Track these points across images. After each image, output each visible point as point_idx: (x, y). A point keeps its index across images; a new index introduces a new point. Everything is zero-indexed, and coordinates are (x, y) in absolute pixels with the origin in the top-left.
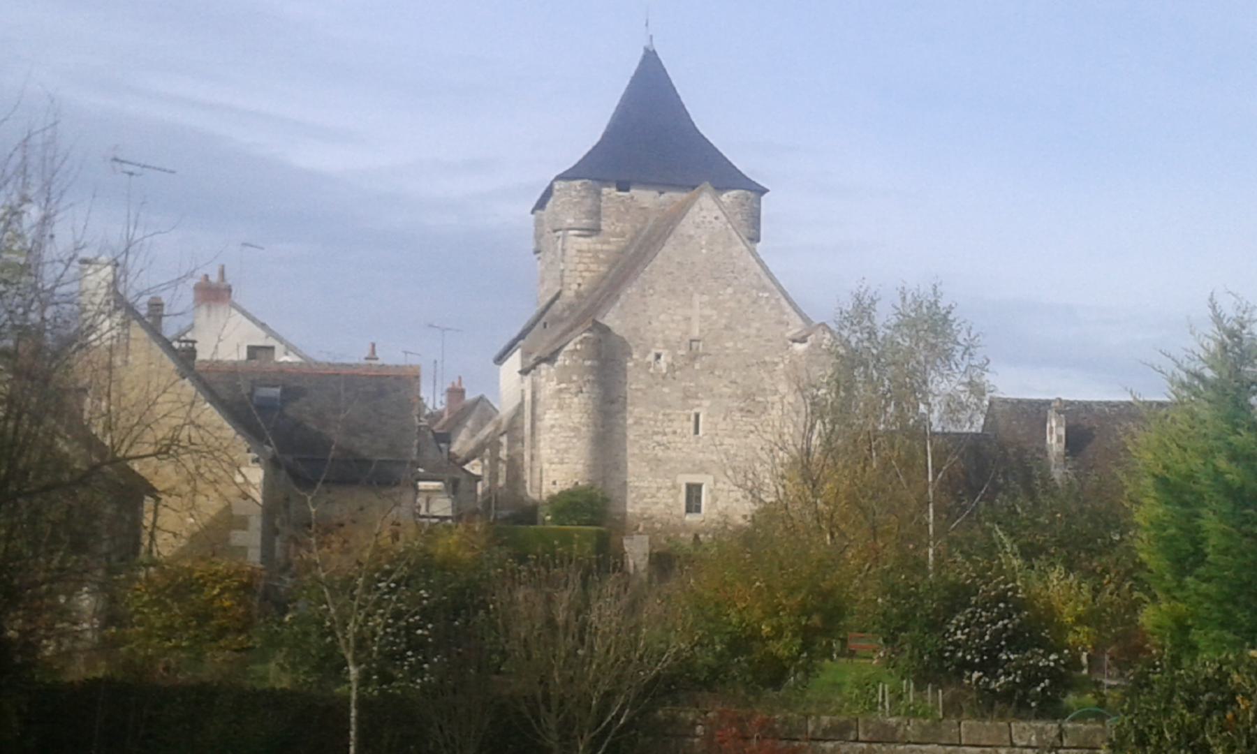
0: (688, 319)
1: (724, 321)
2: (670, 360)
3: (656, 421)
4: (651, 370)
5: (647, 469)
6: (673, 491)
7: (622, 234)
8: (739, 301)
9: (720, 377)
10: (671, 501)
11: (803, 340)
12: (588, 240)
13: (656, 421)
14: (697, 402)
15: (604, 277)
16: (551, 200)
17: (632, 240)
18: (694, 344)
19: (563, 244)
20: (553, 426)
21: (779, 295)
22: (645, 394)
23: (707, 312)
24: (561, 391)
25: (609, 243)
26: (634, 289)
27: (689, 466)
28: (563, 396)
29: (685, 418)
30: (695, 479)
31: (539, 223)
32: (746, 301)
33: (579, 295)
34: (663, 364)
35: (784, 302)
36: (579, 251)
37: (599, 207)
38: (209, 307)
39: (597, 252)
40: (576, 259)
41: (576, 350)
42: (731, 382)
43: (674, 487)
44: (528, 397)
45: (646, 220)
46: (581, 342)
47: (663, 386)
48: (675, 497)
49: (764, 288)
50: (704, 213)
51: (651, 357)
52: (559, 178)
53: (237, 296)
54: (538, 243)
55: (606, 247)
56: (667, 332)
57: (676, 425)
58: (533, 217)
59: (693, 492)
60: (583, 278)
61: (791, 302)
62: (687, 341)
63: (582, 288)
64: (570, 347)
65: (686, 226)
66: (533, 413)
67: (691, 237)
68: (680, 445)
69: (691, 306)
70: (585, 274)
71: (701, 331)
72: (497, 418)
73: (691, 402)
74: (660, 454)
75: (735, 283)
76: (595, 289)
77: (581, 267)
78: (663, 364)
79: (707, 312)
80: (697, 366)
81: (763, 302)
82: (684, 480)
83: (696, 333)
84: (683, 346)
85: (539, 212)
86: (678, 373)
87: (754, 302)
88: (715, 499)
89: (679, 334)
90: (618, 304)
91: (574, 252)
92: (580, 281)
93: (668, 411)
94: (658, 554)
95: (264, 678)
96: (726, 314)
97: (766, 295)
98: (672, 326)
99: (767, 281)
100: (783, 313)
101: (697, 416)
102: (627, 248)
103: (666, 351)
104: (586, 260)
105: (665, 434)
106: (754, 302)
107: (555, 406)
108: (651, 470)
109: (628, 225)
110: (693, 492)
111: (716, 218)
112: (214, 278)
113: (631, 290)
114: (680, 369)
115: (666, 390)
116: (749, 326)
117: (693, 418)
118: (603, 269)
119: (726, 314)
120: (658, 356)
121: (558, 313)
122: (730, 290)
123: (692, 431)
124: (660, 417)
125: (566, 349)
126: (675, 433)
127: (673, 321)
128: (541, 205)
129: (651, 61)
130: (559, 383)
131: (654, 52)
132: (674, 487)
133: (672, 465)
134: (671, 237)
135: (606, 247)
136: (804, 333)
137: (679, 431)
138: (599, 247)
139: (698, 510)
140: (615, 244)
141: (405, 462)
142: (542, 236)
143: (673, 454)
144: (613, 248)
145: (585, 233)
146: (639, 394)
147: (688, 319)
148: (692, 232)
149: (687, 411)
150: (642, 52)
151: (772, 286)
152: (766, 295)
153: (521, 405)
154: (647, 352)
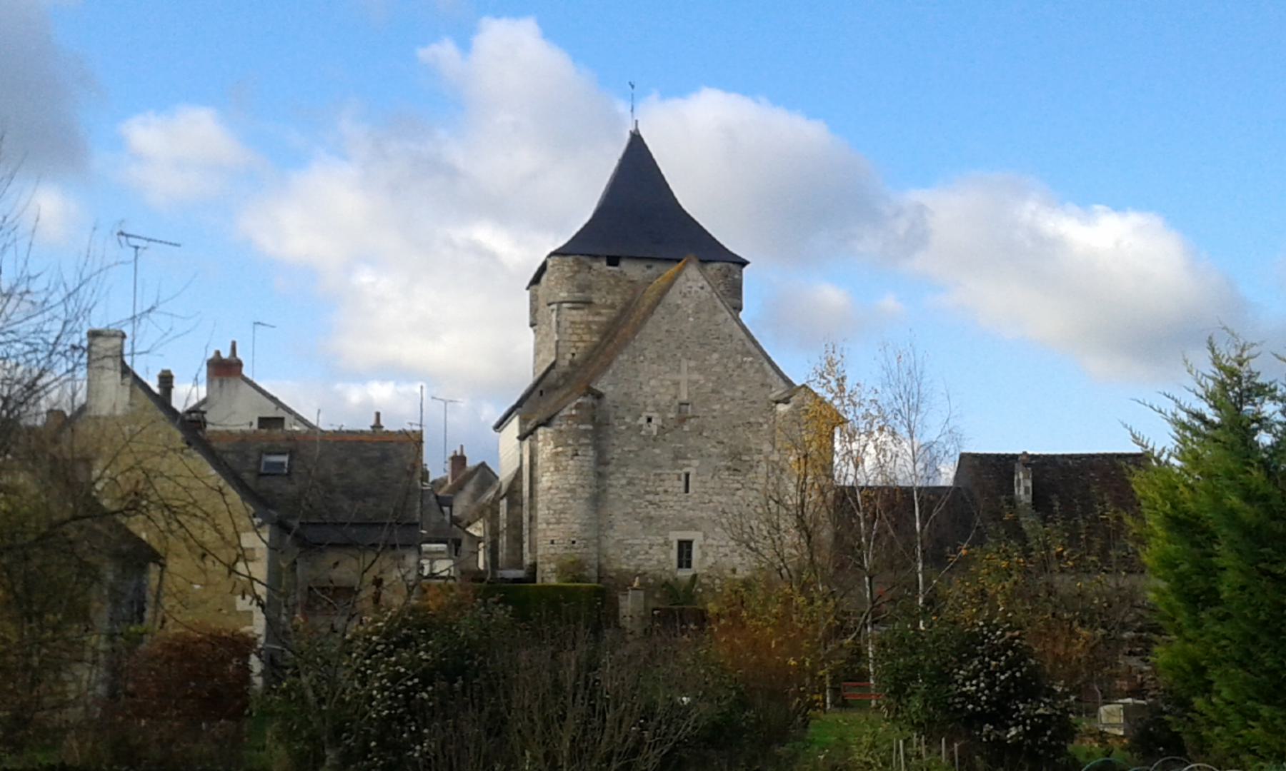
0: (676, 384)
2: (660, 422)
7: (612, 306)
12: (581, 312)
14: (686, 462)
18: (684, 407)
22: (637, 455)
23: (695, 376)
25: (598, 314)
26: (625, 357)
30: (686, 536)
31: (534, 299)
33: (572, 363)
34: (654, 427)
36: (573, 323)
39: (588, 324)
40: (570, 331)
46: (576, 407)
49: (748, 353)
51: (643, 421)
55: (597, 319)
57: (667, 484)
62: (676, 403)
63: (576, 357)
65: (673, 297)
71: (689, 394)
73: (680, 462)
74: (653, 513)
77: (575, 338)
79: (695, 376)
80: (686, 428)
82: (675, 536)
91: (568, 324)
92: (573, 350)
100: (766, 375)
101: (687, 475)
104: (579, 331)
109: (618, 297)
112: (226, 354)
114: (670, 431)
115: (657, 451)
117: (683, 477)
120: (649, 420)
122: (715, 356)
123: (682, 490)
126: (666, 491)
127: (662, 386)
133: (664, 522)
135: (597, 319)
138: (591, 318)
142: (536, 310)
143: (665, 513)
144: (603, 319)
146: (632, 455)
149: (678, 471)
153: (520, 470)
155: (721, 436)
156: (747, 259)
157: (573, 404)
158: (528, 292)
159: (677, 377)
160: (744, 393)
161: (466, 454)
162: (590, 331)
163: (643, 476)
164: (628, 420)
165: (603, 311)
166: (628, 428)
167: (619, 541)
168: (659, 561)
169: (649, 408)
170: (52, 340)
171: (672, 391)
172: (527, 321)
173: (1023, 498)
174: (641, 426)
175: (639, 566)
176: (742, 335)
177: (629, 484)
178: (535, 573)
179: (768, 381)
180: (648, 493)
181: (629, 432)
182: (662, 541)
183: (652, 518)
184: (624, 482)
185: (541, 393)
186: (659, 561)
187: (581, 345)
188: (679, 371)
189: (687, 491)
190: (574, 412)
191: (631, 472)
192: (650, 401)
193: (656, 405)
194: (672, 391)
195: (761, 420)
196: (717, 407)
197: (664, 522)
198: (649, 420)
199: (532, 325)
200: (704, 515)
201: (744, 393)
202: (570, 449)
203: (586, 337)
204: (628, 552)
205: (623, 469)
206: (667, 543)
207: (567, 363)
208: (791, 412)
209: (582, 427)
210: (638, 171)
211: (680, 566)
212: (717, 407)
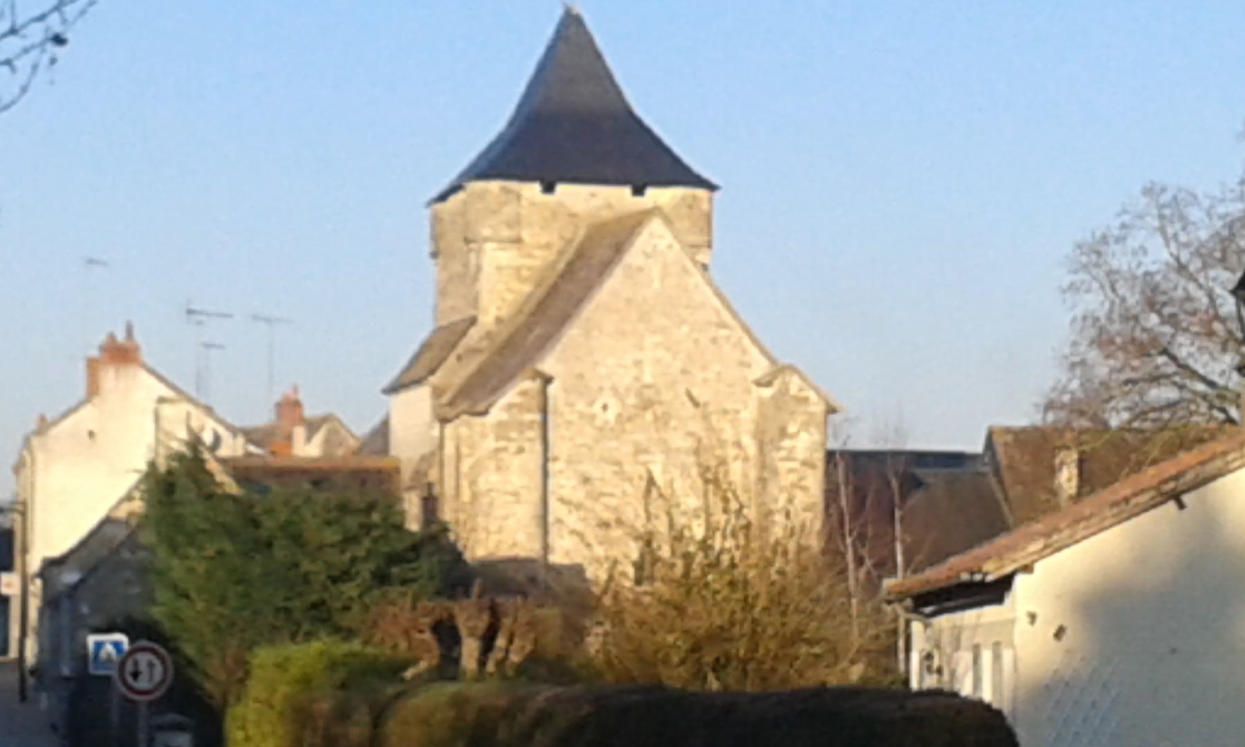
0: (638, 363)
7: (548, 246)
8: (696, 341)
11: (768, 384)
15: (530, 296)
17: (561, 253)
23: (661, 353)
24: (498, 450)
25: (530, 256)
31: (436, 220)
33: (499, 320)
34: (611, 415)
35: (746, 341)
38: (117, 370)
39: (518, 269)
45: (577, 227)
49: (723, 325)
51: (597, 408)
53: (146, 355)
55: (528, 262)
58: (427, 212)
61: (755, 342)
69: (641, 349)
72: (406, 476)
83: (648, 379)
95: (785, 680)
99: (727, 317)
100: (744, 352)
102: (555, 262)
112: (121, 337)
114: (630, 419)
118: (527, 288)
120: (605, 407)
122: (685, 329)
129: (571, 25)
135: (528, 262)
140: (540, 259)
144: (537, 263)
154: (591, 403)
156: (559, 13)
159: (639, 355)
161: (301, 396)
162: (522, 280)
165: (538, 253)
171: (634, 372)
172: (427, 248)
173: (1066, 485)
176: (716, 303)
179: (746, 359)
188: (641, 349)
192: (607, 384)
193: (615, 390)
194: (634, 372)
195: (738, 406)
198: (605, 407)
203: (516, 285)
208: (773, 398)
210: (572, 45)
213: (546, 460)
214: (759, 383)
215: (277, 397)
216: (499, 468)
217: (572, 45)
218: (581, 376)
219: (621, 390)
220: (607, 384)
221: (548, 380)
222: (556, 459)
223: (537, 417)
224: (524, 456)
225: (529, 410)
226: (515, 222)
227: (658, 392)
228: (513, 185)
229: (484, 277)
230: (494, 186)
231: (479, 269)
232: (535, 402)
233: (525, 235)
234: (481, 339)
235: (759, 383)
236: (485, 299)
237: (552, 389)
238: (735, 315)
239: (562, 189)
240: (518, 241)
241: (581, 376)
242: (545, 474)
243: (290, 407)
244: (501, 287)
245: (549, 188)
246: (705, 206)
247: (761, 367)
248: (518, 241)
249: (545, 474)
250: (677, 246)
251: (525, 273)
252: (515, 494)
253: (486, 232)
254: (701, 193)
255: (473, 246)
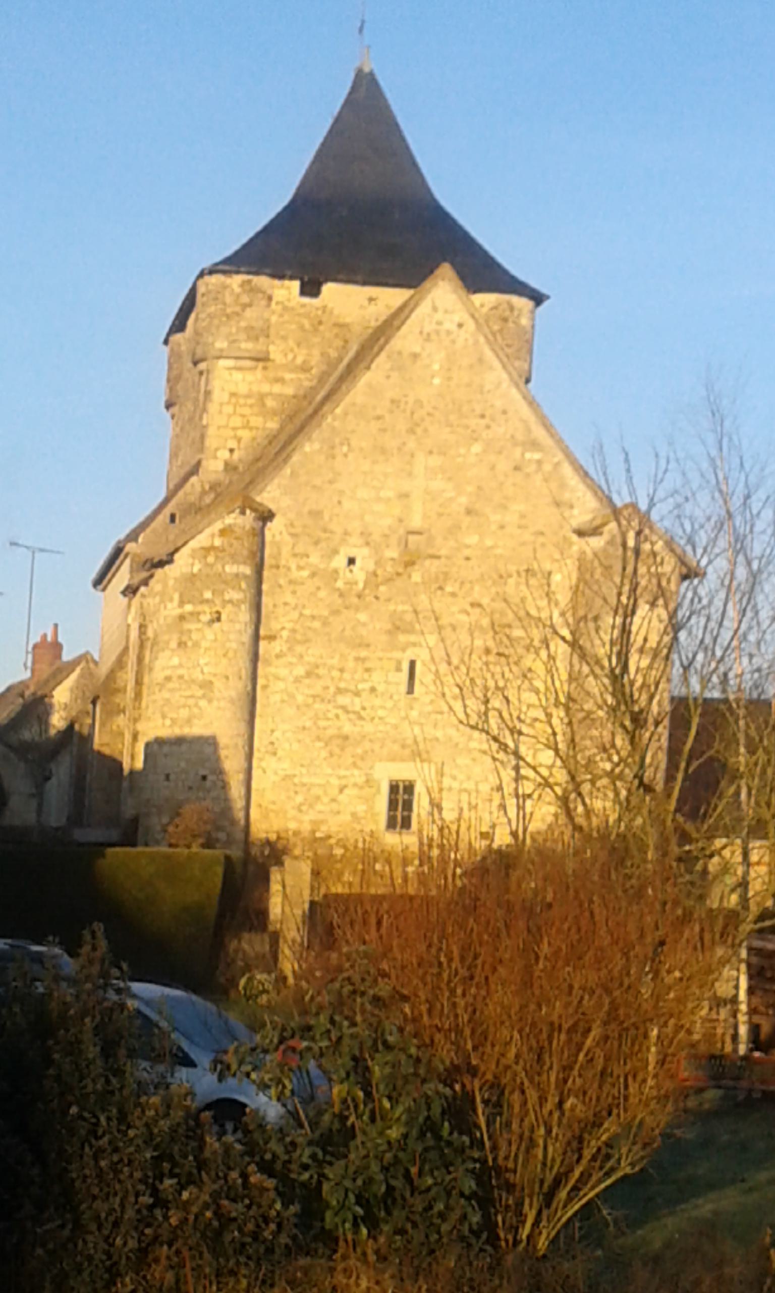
1: (463, 500)
2: (371, 567)
3: (342, 670)
4: (340, 584)
5: (324, 754)
6: (367, 791)
7: (305, 368)
9: (453, 595)
10: (361, 808)
12: (250, 377)
13: (342, 670)
14: (413, 638)
16: (193, 316)
18: (411, 538)
19: (207, 384)
20: (168, 679)
21: (560, 456)
22: (325, 623)
23: (438, 484)
24: (182, 618)
25: (280, 380)
26: (317, 446)
27: (396, 747)
28: (187, 626)
29: (393, 665)
30: (403, 772)
31: (174, 358)
32: (503, 465)
33: (229, 467)
34: (359, 573)
35: (567, 470)
36: (233, 395)
37: (440, 633)
39: (262, 397)
40: (229, 409)
41: (212, 548)
42: (472, 605)
43: (369, 782)
44: (134, 634)
46: (223, 532)
47: (357, 609)
48: (369, 801)
49: (534, 445)
50: (439, 316)
51: (340, 562)
52: (201, 275)
54: (171, 389)
55: (277, 389)
56: (368, 518)
57: (377, 678)
59: (401, 798)
60: (239, 440)
62: (402, 531)
63: (236, 455)
64: (201, 540)
65: (405, 340)
66: (140, 660)
67: (415, 356)
68: (381, 713)
70: (240, 433)
71: (425, 516)
73: (402, 638)
74: (347, 728)
75: (485, 434)
76: (258, 460)
77: (237, 421)
78: (359, 573)
79: (438, 484)
80: (416, 577)
81: (533, 468)
82: (387, 772)
83: (416, 522)
84: (393, 540)
85: (177, 337)
86: (382, 588)
87: (517, 468)
88: (436, 806)
89: (388, 521)
90: (288, 471)
91: (226, 397)
92: (232, 444)
93: (363, 653)
94: (331, 900)
96: (470, 489)
97: (537, 456)
98: (379, 507)
99: (540, 433)
100: (563, 486)
101: (412, 664)
102: (314, 390)
103: (365, 551)
104: (247, 411)
105: (357, 694)
106: (517, 468)
107: (173, 644)
108: (331, 754)
109: (316, 353)
110: (401, 798)
111: (460, 325)
113: (310, 446)
114: (388, 580)
115: (362, 617)
116: (505, 507)
117: (406, 666)
118: (273, 425)
119: (470, 489)
120: (351, 561)
121: (192, 499)
122: (476, 448)
123: (404, 688)
124: (351, 664)
125: (192, 544)
126: (373, 690)
127: (379, 499)
128: (179, 325)
130: (182, 603)
131: (371, 74)
132: (369, 782)
133: (367, 745)
134: (383, 355)
135: (277, 389)
136: (598, 522)
137: (381, 688)
138: (266, 388)
139: (406, 823)
141: (289, 1112)
142: (179, 378)
143: (369, 728)
144: (289, 391)
145: (248, 363)
146: (317, 624)
147: (404, 496)
148: (417, 349)
149: (397, 655)
150: (352, 76)
151: (547, 441)
152: (537, 456)
153: (126, 649)
155: (477, 593)
157: (218, 525)
158: (166, 350)
160: (523, 516)
163: (335, 662)
164: (314, 559)
165: (288, 376)
166: (313, 575)
167: (286, 777)
168: (354, 815)
169: (354, 540)
170: (389, 882)
174: (336, 571)
175: (316, 824)
177: (308, 674)
178: (136, 829)
179: (567, 496)
180: (339, 691)
181: (317, 581)
182: (361, 780)
183: (346, 738)
184: (300, 671)
185: (173, 518)
186: (354, 815)
187: (245, 434)
189: (410, 690)
190: (217, 542)
191: (313, 654)
192: (355, 526)
196: (473, 539)
197: (367, 745)
198: (351, 561)
199: (169, 406)
200: (439, 734)
201: (523, 516)
202: (206, 608)
203: (256, 421)
204: (299, 799)
205: (299, 649)
206: (369, 782)
207: (220, 466)
209: (231, 569)
210: (365, 121)
211: (391, 824)
212: (473, 539)
213: (256, 637)
214: (580, 533)
215: (36, 639)
216: (181, 644)
217: (365, 121)
218: (316, 514)
219: (376, 537)
220: (355, 526)
221: (266, 516)
222: (272, 638)
223: (247, 570)
224: (224, 625)
225: (234, 559)
226: (263, 332)
227: (431, 540)
228: (263, 281)
229: (213, 408)
230: (236, 281)
231: (208, 393)
232: (244, 547)
233: (275, 353)
234: (204, 493)
235: (580, 533)
236: (211, 442)
237: (273, 529)
238: (547, 426)
239: (329, 289)
240: (262, 359)
241: (316, 514)
242: (255, 658)
243: (48, 649)
244: (237, 421)
245: (311, 289)
246: (524, 321)
247: (586, 507)
248: (262, 359)
249: (255, 658)
250: (470, 325)
251: (270, 403)
252: (207, 685)
253: (221, 344)
254: (522, 303)
255: (202, 366)
